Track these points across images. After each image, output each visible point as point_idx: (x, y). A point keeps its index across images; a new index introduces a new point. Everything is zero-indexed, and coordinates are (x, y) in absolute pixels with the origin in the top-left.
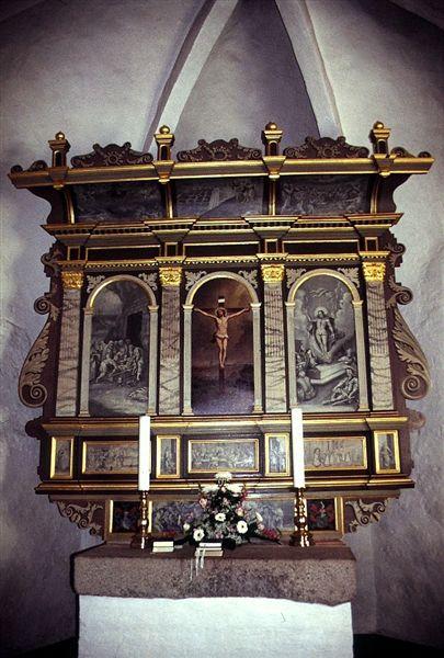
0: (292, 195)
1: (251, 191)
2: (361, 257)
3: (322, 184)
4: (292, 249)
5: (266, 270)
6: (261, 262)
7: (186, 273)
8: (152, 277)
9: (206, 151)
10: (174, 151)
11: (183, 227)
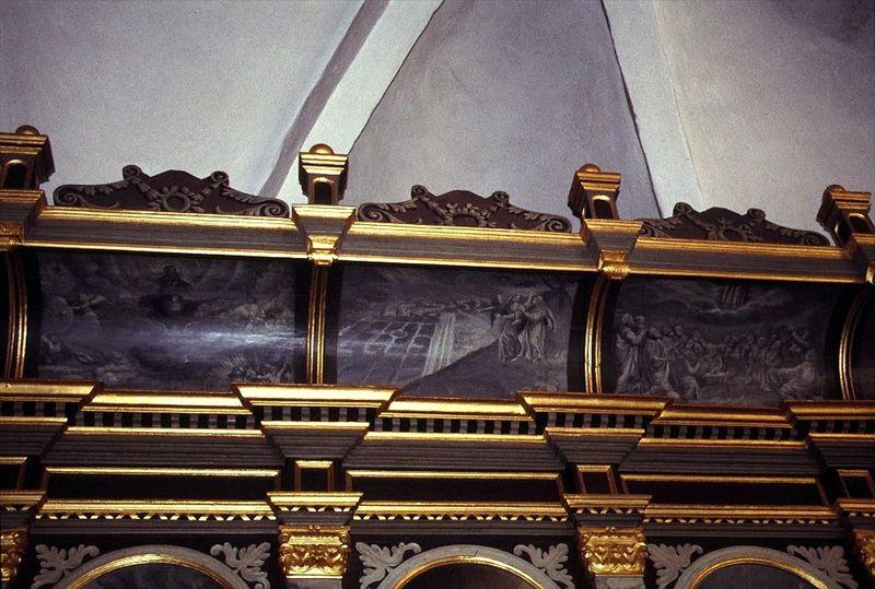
0: (641, 346)
1: (537, 331)
2: (845, 514)
3: (716, 320)
4: (662, 493)
5: (595, 541)
6: (283, 516)
7: (360, 546)
8: (257, 554)
9: (424, 207)
10: (357, 193)
11: (353, 414)
